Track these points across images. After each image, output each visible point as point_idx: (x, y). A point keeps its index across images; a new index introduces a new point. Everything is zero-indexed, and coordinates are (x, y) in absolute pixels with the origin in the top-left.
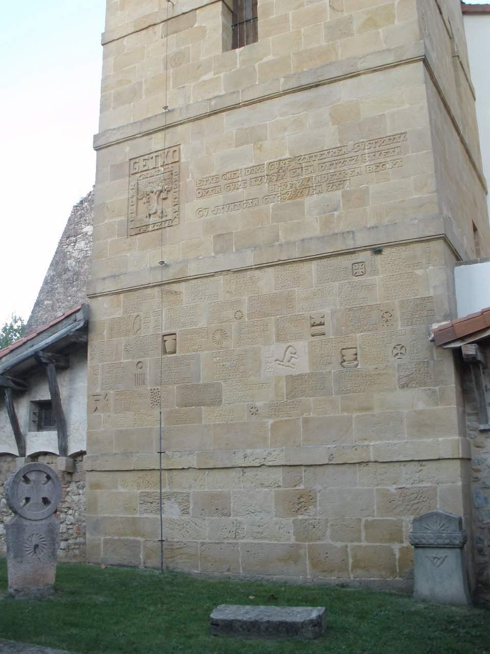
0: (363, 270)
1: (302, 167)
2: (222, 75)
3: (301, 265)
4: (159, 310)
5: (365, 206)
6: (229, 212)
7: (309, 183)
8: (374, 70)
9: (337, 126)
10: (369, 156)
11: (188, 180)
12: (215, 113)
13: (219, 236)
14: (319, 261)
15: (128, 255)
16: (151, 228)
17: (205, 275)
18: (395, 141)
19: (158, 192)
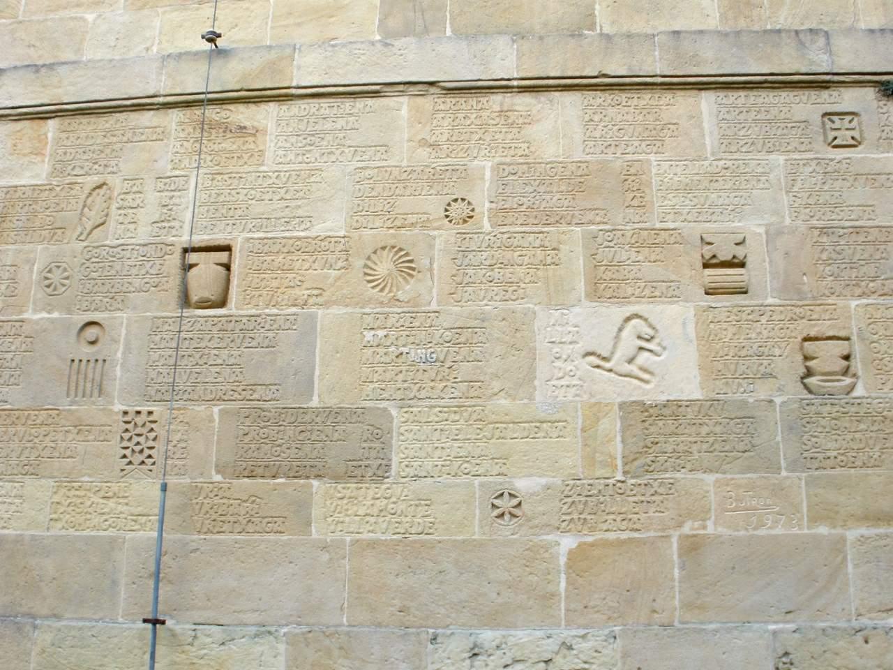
0: (856, 134)
3: (667, 97)
4: (177, 173)
14: (722, 94)
15: (90, 17)
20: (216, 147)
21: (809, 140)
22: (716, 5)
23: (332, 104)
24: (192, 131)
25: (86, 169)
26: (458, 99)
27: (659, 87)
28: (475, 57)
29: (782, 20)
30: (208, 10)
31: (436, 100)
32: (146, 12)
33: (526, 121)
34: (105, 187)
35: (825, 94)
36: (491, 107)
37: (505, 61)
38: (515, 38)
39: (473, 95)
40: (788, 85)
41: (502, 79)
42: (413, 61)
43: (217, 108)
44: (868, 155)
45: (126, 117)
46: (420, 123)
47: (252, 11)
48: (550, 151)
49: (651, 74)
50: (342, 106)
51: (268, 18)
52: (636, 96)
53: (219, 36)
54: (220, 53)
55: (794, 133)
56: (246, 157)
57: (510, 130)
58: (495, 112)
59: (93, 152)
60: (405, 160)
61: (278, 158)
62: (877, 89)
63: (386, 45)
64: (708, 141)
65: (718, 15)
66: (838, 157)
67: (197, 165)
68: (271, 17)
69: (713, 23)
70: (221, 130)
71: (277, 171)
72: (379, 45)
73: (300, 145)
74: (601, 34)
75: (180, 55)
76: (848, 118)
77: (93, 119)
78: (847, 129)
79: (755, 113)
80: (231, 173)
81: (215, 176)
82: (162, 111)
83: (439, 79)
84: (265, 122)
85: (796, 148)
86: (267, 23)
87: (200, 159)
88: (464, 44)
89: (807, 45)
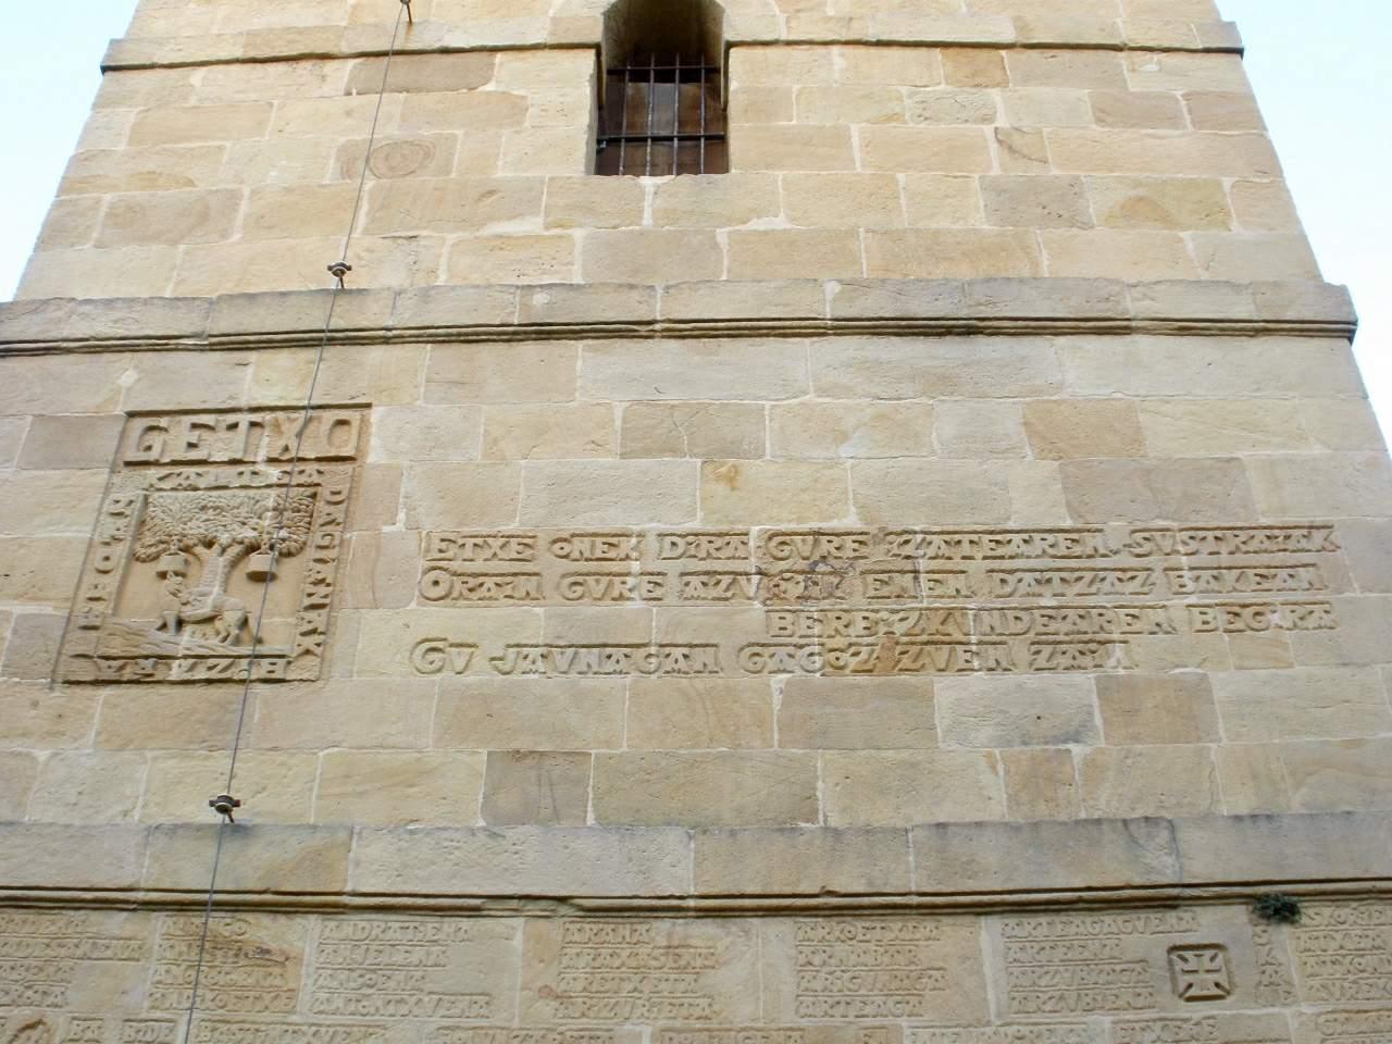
0: (1222, 978)
1: (916, 572)
2: (578, 234)
3: (928, 926)
4: (158, 1014)
5: (1199, 739)
6: (573, 675)
7: (950, 628)
8: (1186, 328)
9: (1057, 463)
10: (1198, 578)
11: (386, 529)
12: (543, 332)
13: (518, 755)
14: (1012, 920)
15: (42, 755)
16: (176, 671)
17: (432, 901)
18: (1291, 545)
19: (237, 549)
20: (222, 979)
21: (1150, 990)
22: (1002, 782)
23: (406, 925)
24: (185, 949)
25: (13, 995)
26: (601, 926)
27: (914, 911)
28: (630, 860)
29: (1102, 803)
30: (222, 761)
31: (567, 926)
32: (127, 755)
33: (707, 963)
34: (41, 1027)
35: (1171, 917)
36: (653, 939)
37: (677, 869)
38: (692, 832)
39: (626, 920)
40: (1114, 905)
41: (671, 897)
42: (534, 863)
43: (227, 917)
44: (1241, 1011)
45: (83, 918)
46: (541, 961)
47: (290, 769)
48: (744, 1012)
49: (902, 891)
50: (421, 928)
51: (313, 780)
52: (878, 925)
53: (237, 804)
54: (237, 830)
55: (1124, 979)
56: (267, 997)
57: (683, 976)
58: (659, 948)
59: (27, 970)
60: (517, 1020)
61: (318, 1003)
62: (1251, 908)
63: (494, 835)
64: (991, 995)
65: (1005, 796)
66: (1196, 1017)
67: (188, 1005)
68: (317, 781)
69: (998, 810)
70: (231, 953)
71: (314, 1025)
72: (482, 836)
73: (353, 985)
74: (826, 829)
75: (174, 830)
76: (1208, 953)
77: (31, 916)
78: (1208, 971)
79: (1065, 950)
80: (243, 1022)
81: (219, 1025)
82: (141, 914)
83: (575, 894)
84: (300, 944)
85: (1129, 1003)
86: (311, 789)
87: (195, 996)
88: (613, 838)
89: (1141, 842)
